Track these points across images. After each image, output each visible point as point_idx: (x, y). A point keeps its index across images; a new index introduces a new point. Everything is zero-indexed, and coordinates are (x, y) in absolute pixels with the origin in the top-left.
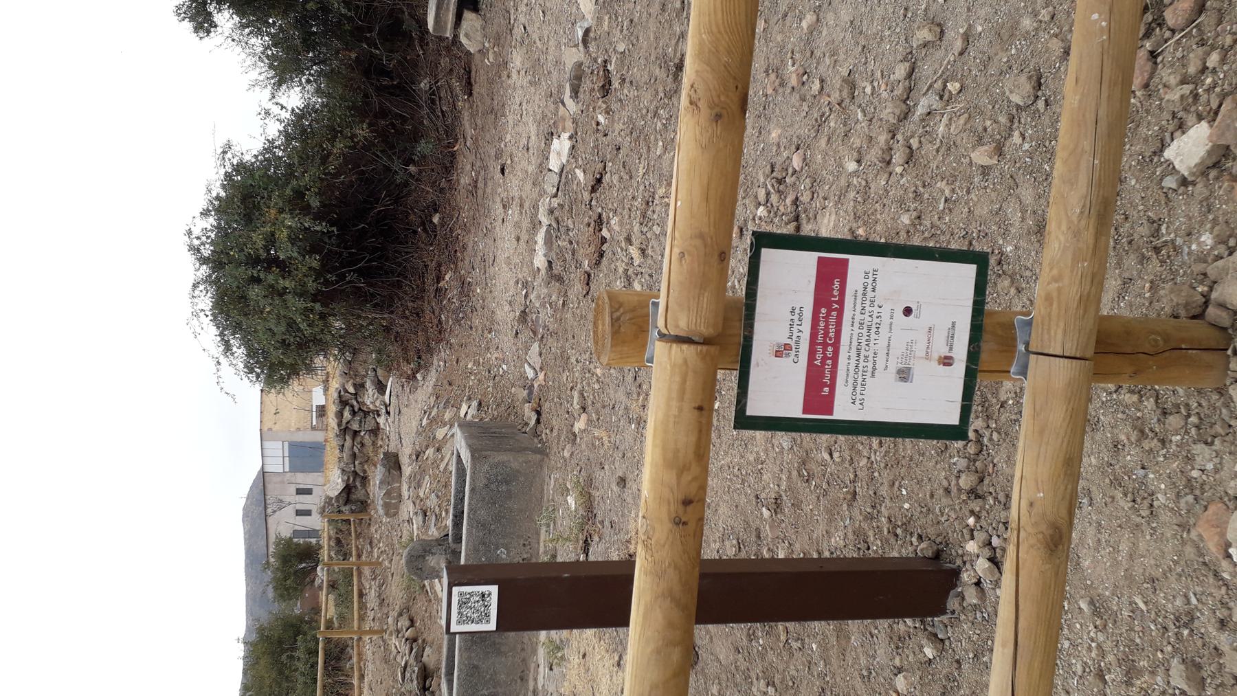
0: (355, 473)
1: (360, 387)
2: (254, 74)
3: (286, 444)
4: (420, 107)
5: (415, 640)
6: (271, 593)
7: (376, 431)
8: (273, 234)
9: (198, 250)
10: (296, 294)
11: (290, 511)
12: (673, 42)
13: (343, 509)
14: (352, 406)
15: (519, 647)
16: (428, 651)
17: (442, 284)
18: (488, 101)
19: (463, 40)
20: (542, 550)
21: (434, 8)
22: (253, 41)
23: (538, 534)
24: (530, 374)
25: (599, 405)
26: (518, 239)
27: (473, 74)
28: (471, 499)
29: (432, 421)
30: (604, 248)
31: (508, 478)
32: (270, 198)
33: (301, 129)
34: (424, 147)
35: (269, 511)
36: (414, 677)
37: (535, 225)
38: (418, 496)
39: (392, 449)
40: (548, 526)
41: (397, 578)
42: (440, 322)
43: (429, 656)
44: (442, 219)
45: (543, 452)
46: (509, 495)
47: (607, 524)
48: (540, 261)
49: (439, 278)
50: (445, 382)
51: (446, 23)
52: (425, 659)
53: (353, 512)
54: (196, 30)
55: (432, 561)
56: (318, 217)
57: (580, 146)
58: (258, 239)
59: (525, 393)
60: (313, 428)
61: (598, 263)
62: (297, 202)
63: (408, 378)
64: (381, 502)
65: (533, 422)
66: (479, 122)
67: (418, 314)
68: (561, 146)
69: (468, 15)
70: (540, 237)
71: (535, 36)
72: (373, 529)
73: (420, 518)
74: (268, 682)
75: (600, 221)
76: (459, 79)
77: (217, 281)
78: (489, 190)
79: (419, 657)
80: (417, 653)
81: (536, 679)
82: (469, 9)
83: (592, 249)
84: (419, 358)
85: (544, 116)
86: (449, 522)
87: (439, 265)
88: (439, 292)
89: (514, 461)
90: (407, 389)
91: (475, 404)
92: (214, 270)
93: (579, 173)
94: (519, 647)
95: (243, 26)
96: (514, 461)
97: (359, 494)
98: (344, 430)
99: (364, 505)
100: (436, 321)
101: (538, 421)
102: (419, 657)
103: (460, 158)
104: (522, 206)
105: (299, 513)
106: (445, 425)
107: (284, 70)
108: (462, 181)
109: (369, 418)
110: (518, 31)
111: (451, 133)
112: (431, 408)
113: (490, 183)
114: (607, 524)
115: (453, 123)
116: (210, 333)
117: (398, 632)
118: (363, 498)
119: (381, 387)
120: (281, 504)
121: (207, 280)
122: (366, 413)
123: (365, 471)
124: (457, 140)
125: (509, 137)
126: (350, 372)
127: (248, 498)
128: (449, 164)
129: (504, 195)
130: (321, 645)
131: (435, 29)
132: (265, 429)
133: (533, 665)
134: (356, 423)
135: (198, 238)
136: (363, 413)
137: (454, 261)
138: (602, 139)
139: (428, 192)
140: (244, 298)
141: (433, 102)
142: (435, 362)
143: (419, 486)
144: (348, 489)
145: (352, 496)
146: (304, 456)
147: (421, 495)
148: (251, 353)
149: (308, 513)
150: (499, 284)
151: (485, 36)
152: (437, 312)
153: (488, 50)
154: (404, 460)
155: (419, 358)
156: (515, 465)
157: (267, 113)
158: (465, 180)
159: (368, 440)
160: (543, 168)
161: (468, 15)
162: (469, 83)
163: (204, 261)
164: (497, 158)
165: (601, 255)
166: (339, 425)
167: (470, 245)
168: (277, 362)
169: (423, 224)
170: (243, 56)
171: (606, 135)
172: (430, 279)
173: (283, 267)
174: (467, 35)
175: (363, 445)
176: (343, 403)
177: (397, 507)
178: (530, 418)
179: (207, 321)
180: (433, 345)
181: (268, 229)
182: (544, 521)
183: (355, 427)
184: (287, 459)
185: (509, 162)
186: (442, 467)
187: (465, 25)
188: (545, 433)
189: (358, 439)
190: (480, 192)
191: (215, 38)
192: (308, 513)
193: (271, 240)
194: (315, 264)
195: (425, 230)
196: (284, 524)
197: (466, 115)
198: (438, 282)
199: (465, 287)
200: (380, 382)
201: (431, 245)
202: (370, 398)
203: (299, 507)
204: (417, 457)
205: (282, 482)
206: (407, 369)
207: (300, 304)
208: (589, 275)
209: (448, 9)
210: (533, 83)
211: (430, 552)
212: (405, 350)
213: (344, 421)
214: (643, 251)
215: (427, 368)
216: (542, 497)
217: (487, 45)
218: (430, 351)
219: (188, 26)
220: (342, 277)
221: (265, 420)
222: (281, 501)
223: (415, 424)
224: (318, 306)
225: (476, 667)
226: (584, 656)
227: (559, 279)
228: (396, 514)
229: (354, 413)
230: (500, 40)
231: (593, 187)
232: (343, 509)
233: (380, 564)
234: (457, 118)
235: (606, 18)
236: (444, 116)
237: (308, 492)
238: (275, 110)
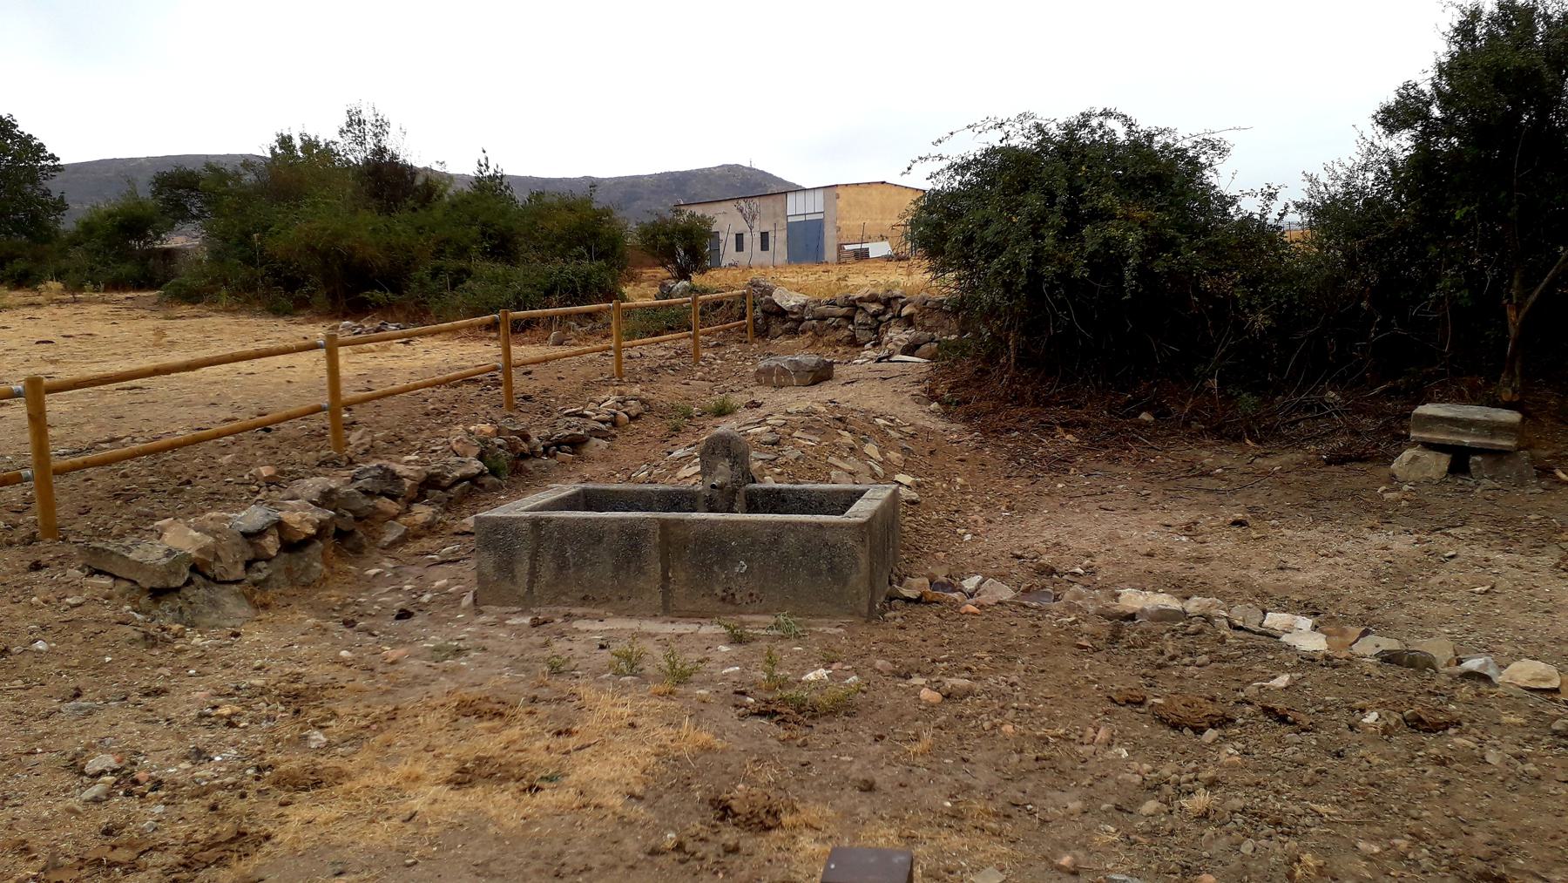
0: (802, 320)
1: (909, 321)
2: (1324, 178)
3: (821, 216)
4: (1299, 393)
5: (615, 424)
6: (648, 220)
7: (854, 343)
8: (1113, 217)
9: (1085, 125)
10: (1036, 251)
11: (742, 226)
12: (1535, 868)
13: (758, 309)
14: (884, 313)
15: (625, 593)
16: (604, 444)
17: (1059, 429)
18: (1327, 492)
19: (1408, 454)
20: (745, 618)
21: (1449, 414)
22: (1371, 176)
23: (766, 612)
24: (970, 584)
25: (960, 728)
26: (1150, 555)
27: (1358, 466)
28: (809, 524)
29: (881, 431)
30: (1187, 732)
31: (837, 573)
32: (1160, 209)
33: (1257, 237)
34: (1248, 402)
35: (742, 203)
36: (572, 431)
37: (1181, 587)
38: (794, 429)
39: (837, 369)
40: (777, 625)
41: (683, 390)
42: (1008, 431)
43: (598, 445)
44: (1147, 425)
45: (873, 616)
46: (815, 573)
47: (806, 756)
48: (1133, 599)
49: (1068, 427)
50: (933, 445)
51: (1430, 431)
52: (594, 441)
53: (755, 321)
54: (1387, 111)
55: (723, 466)
56: (1143, 272)
57: (1315, 675)
58: (1107, 200)
59: (942, 578)
60: (840, 247)
61: (1162, 720)
62: (1157, 243)
63: (931, 390)
64: (773, 364)
65: (906, 593)
66: (1293, 477)
67: (1019, 399)
68: (1307, 638)
69: (1444, 461)
70: (1172, 603)
71: (1444, 575)
72: (735, 347)
73: (770, 438)
74: (549, 225)
75: (1224, 722)
76: (1347, 448)
77: (1044, 150)
78: (1202, 497)
79: (596, 433)
80: (600, 430)
81: (584, 617)
82: (1453, 460)
83: (1183, 712)
84: (958, 404)
85: (1337, 598)
86: (770, 483)
87: (1085, 425)
88: (1048, 429)
89: (858, 580)
90: (916, 390)
91: (914, 496)
92: (1059, 146)
93: (1282, 680)
94: (625, 593)
95: (1392, 163)
96: (858, 580)
97: (776, 327)
98: (854, 305)
99: (762, 333)
100: (1008, 425)
101: (908, 600)
102: (596, 433)
103: (1235, 449)
104: (1198, 560)
105: (739, 238)
106: (882, 453)
107: (1333, 215)
108: (1205, 453)
109: (870, 334)
110: (1440, 542)
111: (1268, 434)
112: (897, 428)
113: (1211, 498)
114: (806, 756)
115: (1282, 437)
116: (972, 146)
117: (623, 402)
118: (772, 331)
119: (911, 349)
120: (750, 218)
121: (1046, 138)
122: (876, 330)
123: (804, 332)
124: (1259, 442)
125: (1289, 533)
126: (930, 309)
127: (750, 169)
128: (1226, 432)
129: (1203, 527)
130: (603, 305)
131: (1419, 416)
132: (839, 191)
133: (602, 612)
134: (860, 321)
135: (1101, 125)
136: (877, 328)
137: (1094, 445)
138: (1342, 717)
139: (1183, 405)
140: (1025, 187)
141: (1309, 409)
142: (955, 427)
143: (806, 429)
144: (781, 313)
145: (771, 320)
146: (807, 242)
147: (796, 434)
148: (953, 196)
149: (740, 247)
150: (1078, 521)
151: (1417, 484)
152: (1022, 426)
153: (1398, 489)
154: (826, 392)
155: (958, 404)
156: (854, 579)
157: (1272, 196)
158: (1207, 457)
159: (843, 334)
160: (1266, 599)
161: (1444, 461)
162: (1348, 459)
163: (1070, 130)
164: (1251, 510)
165: (1175, 726)
166: (861, 299)
167: (1119, 469)
168: (941, 225)
169: (1137, 399)
170: (1349, 164)
171: (1351, 728)
172: (1063, 412)
173: (1071, 231)
174: (1415, 458)
175: (836, 328)
176: (888, 302)
177: (768, 383)
178: (909, 587)
179: (994, 139)
180: (976, 421)
181: (1119, 210)
182: (782, 619)
183: (859, 318)
184: (802, 219)
185: (1254, 534)
186: (833, 460)
187: (1429, 456)
188: (895, 616)
189: (844, 323)
190: (1196, 482)
191: (1375, 133)
192: (740, 247)
193: (1105, 215)
194: (1077, 273)
195: (1129, 403)
196: (726, 221)
197: (1298, 456)
198: (1062, 425)
199: (1060, 465)
200: (918, 347)
201: (1110, 412)
202: (897, 335)
203: (747, 237)
204: (840, 419)
205: (775, 215)
206: (942, 389)
207: (1025, 260)
208: (1141, 704)
209: (1452, 433)
210: (1376, 576)
211: (734, 464)
212: (966, 384)
213: (864, 305)
214: (1204, 816)
215: (947, 415)
216: (812, 616)
217: (1406, 488)
218: (968, 419)
219: (1391, 98)
220: (1061, 305)
221: (850, 190)
222: (754, 218)
223: (874, 403)
224: (1022, 281)
225: (600, 541)
226: (632, 725)
227: (1115, 637)
228: (759, 383)
229: (875, 315)
230: (1418, 511)
231: (1273, 709)
232: (758, 309)
233: (696, 362)
234: (1292, 443)
235: (1519, 720)
236: (1292, 423)
237: (764, 246)
238: (1277, 207)
